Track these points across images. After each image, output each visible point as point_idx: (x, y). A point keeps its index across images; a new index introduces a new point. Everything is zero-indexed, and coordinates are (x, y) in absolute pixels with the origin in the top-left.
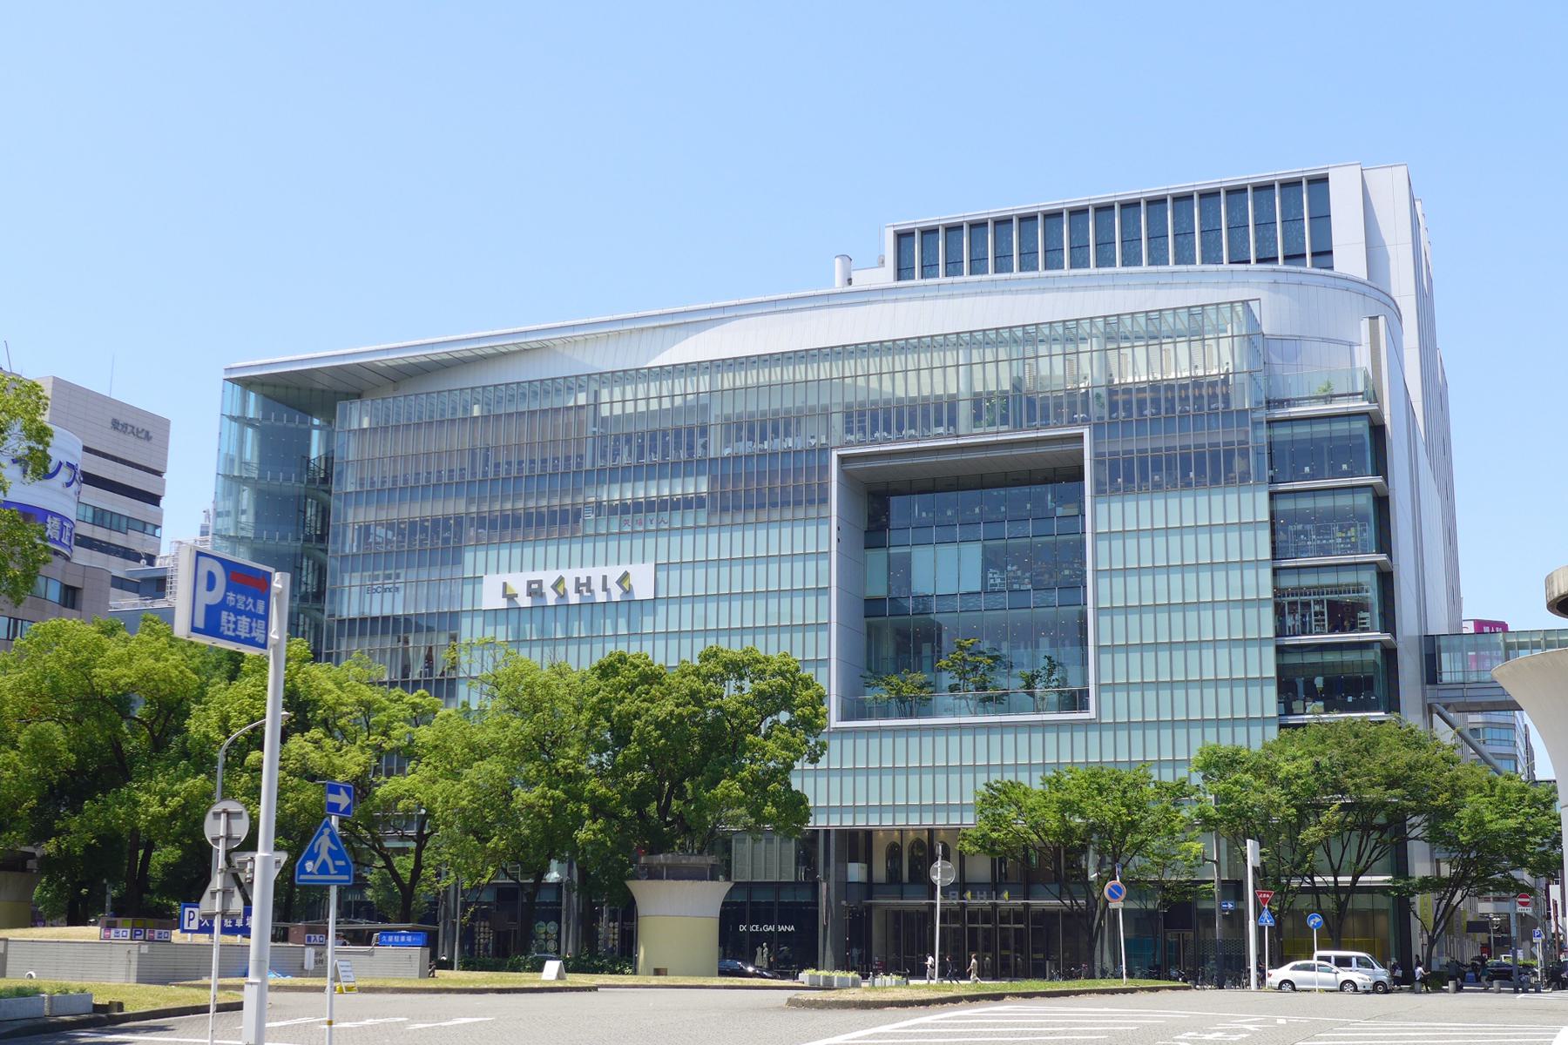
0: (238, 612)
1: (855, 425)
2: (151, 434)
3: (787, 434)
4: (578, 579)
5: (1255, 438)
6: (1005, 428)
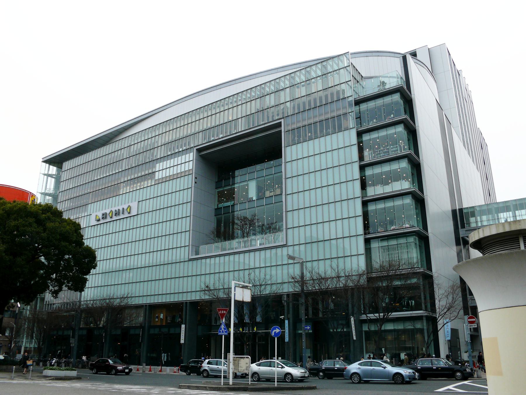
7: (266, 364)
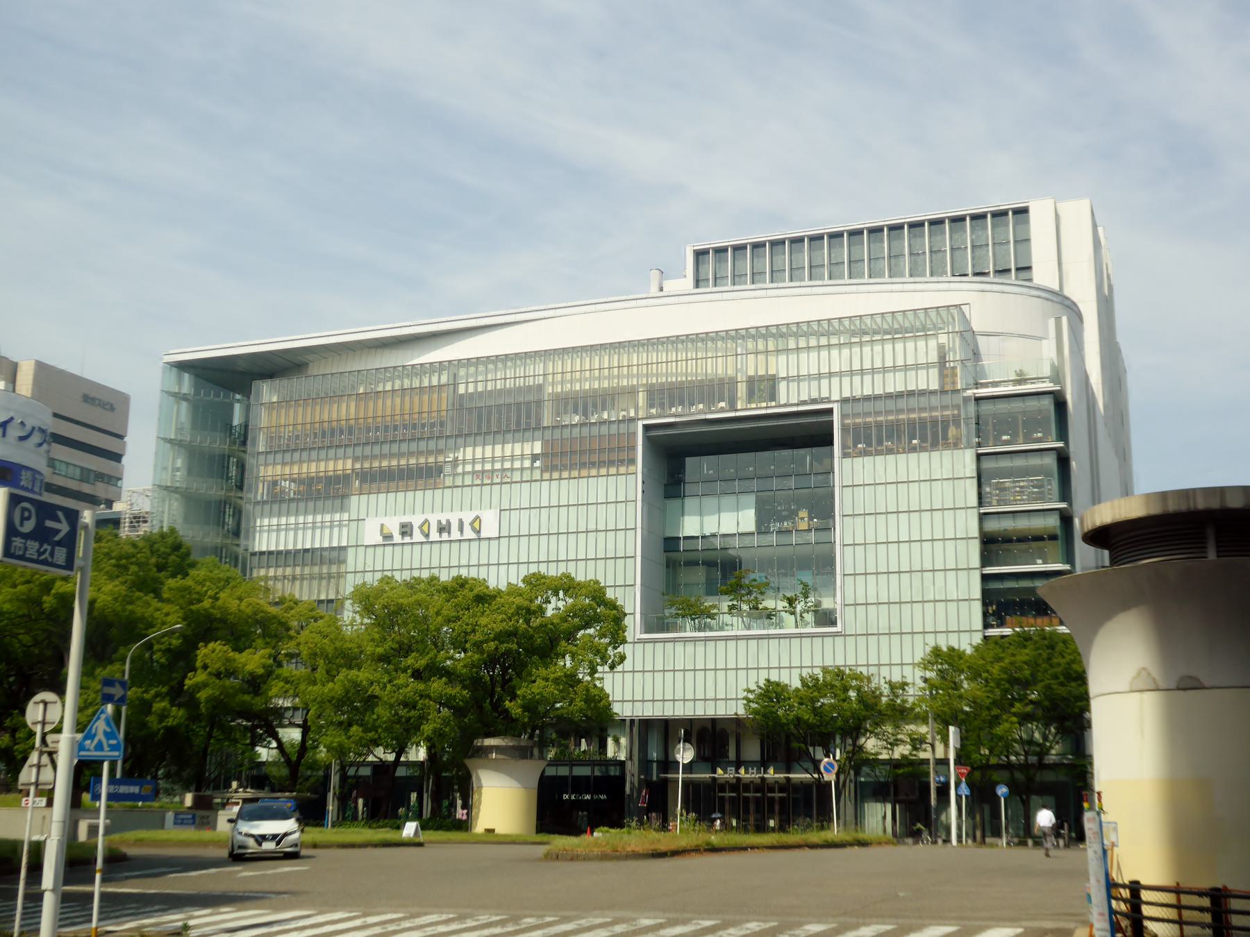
3: (604, 409)
4: (439, 522)
5: (966, 412)
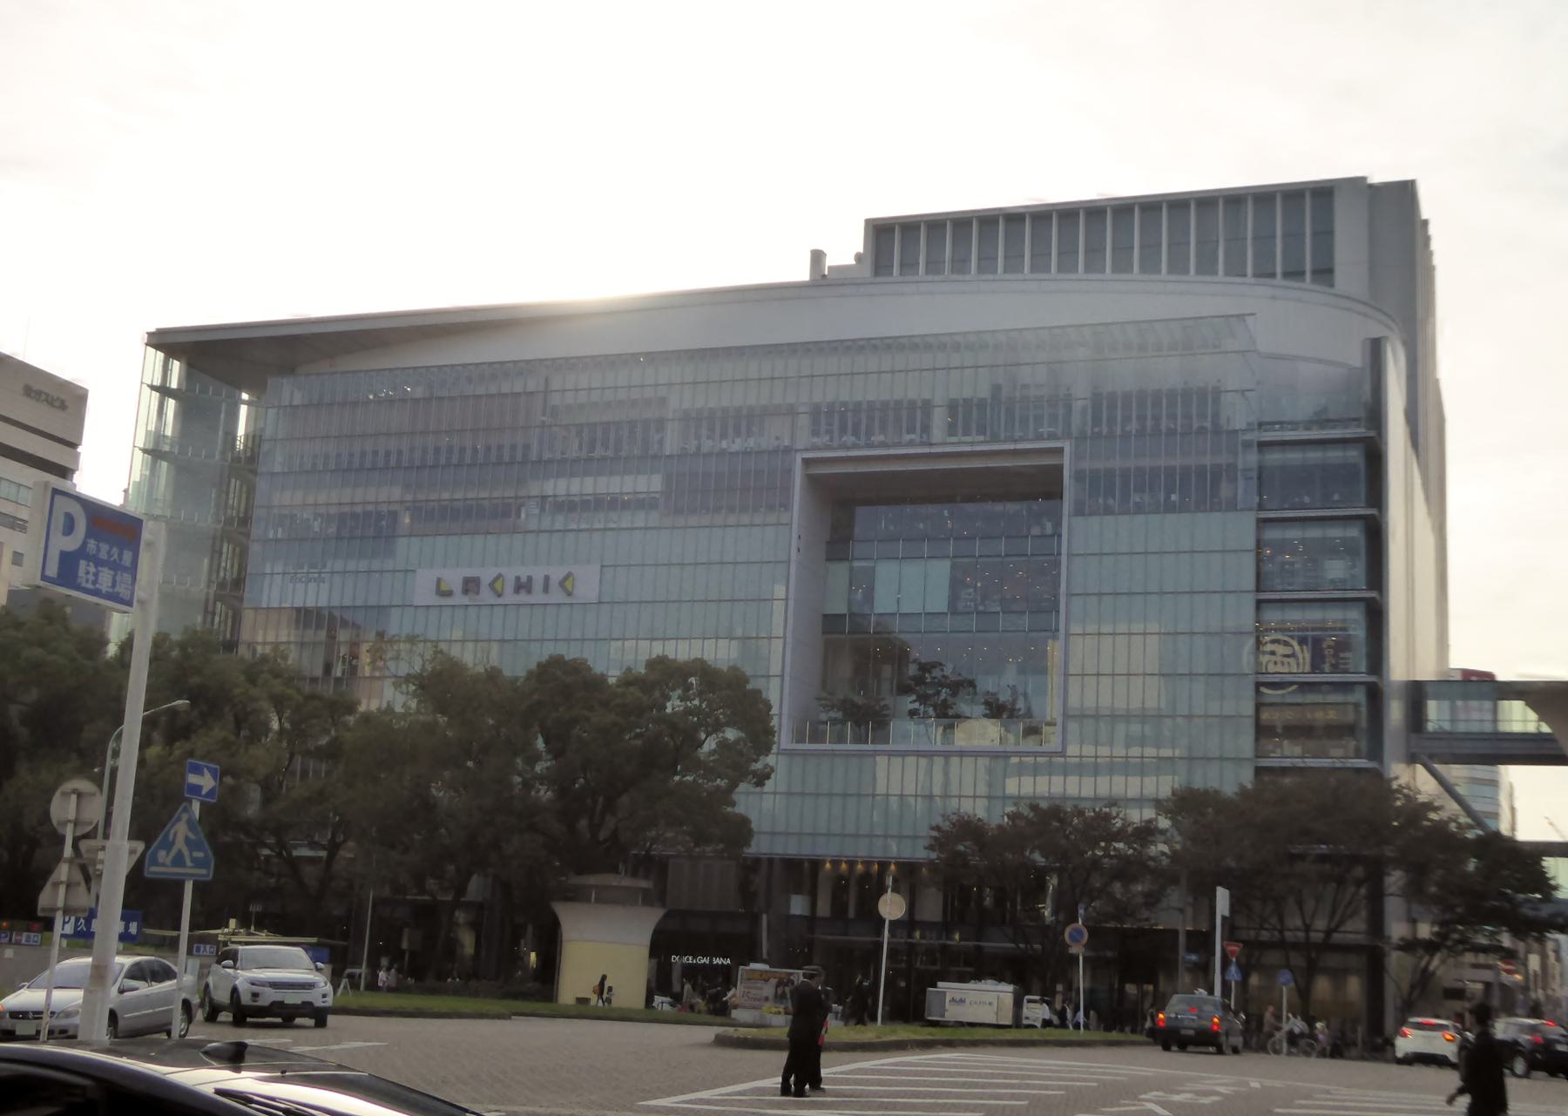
0: (99, 563)
1: (823, 427)
2: (67, 404)
3: (749, 434)
4: (518, 578)
6: (981, 438)
7: (297, 1069)
